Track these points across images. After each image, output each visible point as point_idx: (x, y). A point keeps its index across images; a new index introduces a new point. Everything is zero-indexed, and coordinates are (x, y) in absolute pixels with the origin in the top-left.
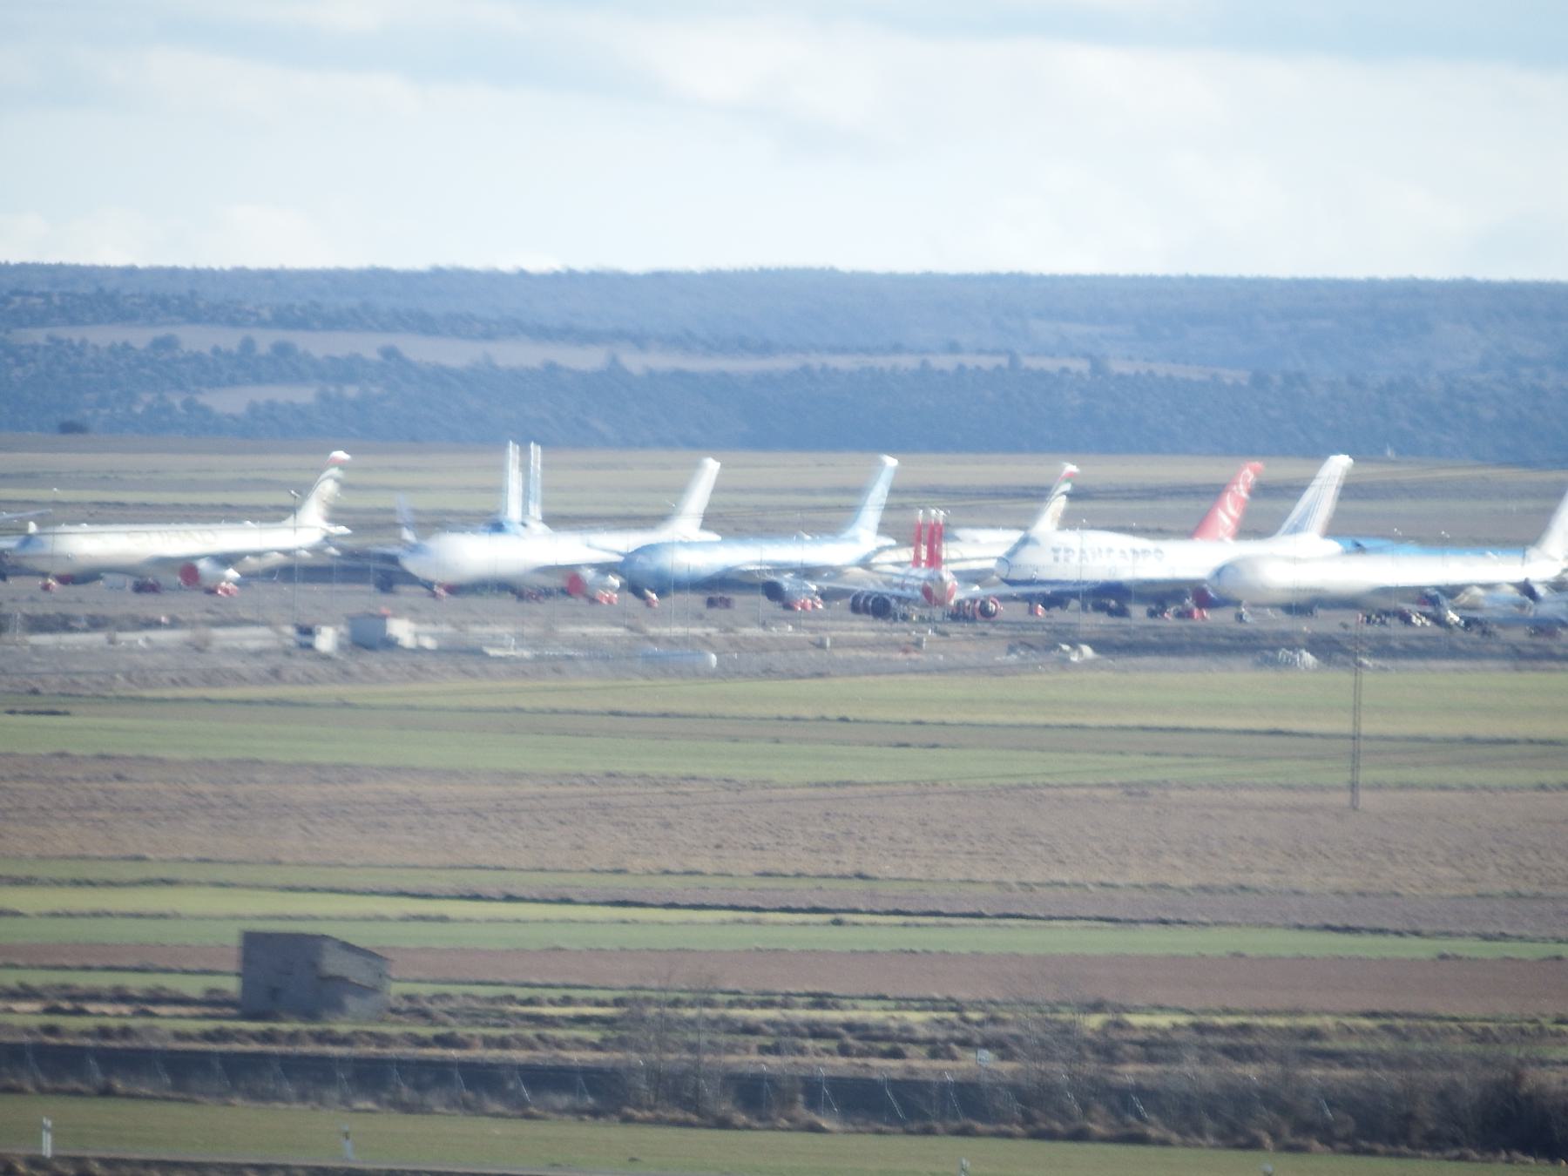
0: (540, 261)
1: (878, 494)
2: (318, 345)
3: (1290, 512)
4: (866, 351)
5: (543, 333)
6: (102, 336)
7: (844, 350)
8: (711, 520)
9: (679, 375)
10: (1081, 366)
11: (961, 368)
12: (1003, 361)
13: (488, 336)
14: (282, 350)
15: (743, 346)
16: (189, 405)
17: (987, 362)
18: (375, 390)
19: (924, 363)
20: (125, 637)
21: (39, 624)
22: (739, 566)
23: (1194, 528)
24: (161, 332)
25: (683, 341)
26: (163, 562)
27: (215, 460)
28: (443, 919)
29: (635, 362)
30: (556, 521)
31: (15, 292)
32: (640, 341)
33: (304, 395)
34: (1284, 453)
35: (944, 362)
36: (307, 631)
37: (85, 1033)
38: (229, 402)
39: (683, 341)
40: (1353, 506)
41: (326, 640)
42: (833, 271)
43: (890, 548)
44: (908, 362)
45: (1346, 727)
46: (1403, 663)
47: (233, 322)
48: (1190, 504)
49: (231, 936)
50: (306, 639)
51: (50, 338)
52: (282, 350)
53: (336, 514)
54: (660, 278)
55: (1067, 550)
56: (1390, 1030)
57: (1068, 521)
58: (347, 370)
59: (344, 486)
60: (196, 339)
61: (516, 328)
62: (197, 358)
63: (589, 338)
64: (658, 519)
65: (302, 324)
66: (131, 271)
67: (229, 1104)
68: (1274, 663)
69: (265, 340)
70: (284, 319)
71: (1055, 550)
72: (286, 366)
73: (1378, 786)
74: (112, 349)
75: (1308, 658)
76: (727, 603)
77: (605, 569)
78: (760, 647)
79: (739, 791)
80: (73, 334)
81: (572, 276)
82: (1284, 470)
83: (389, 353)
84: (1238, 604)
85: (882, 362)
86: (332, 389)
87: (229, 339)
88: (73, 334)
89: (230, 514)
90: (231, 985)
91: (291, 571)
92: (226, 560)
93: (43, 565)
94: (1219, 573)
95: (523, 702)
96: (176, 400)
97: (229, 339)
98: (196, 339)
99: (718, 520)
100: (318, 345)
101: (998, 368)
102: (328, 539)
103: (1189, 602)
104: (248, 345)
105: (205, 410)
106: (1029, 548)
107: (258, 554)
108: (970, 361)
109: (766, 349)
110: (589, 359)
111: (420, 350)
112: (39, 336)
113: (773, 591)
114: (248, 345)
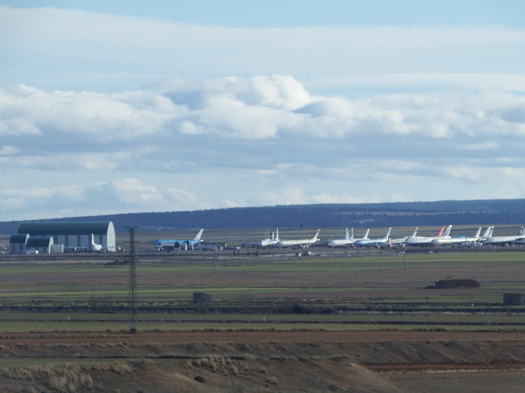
2: (374, 213)
4: (449, 211)
6: (345, 213)
7: (446, 211)
8: (368, 237)
9: (423, 216)
10: (478, 212)
11: (462, 213)
12: (467, 212)
13: (398, 211)
15: (432, 211)
16: (356, 222)
17: (465, 212)
18: (382, 219)
19: (414, 214)
20: (275, 255)
21: (263, 254)
22: (98, 245)
23: (473, 236)
27: (339, 230)
28: (253, 290)
29: (417, 214)
30: (330, 237)
32: (419, 211)
34: (425, 225)
35: (460, 213)
36: (297, 254)
37: (162, 306)
39: (425, 211)
40: (452, 232)
41: (300, 255)
42: (454, 200)
43: (369, 240)
44: (455, 213)
45: (403, 261)
46: (449, 252)
48: (437, 232)
49: (192, 294)
50: (297, 255)
51: (384, 214)
52: (370, 214)
53: (318, 238)
55: (414, 239)
56: (33, 301)
57: (417, 235)
58: (379, 217)
61: (401, 210)
63: (412, 211)
64: (362, 237)
66: (361, 204)
67: (215, 314)
68: (427, 253)
69: (367, 213)
70: (370, 210)
71: (413, 239)
72: (370, 216)
75: (432, 252)
76: (369, 248)
78: (361, 253)
79: (214, 272)
80: (341, 213)
82: (485, 226)
83: (384, 214)
84: (435, 245)
85: (451, 213)
86: (376, 220)
87: (363, 213)
88: (341, 213)
89: (305, 238)
90: (192, 299)
91: (313, 246)
92: (304, 244)
94: (432, 241)
96: (355, 222)
97: (363, 213)
98: (358, 213)
100: (374, 213)
102: (317, 241)
103: (431, 245)
104: (365, 214)
106: (409, 239)
108: (463, 212)
109: (435, 212)
110: (411, 214)
111: (388, 214)
112: (337, 214)
113: (375, 246)
114: (365, 214)
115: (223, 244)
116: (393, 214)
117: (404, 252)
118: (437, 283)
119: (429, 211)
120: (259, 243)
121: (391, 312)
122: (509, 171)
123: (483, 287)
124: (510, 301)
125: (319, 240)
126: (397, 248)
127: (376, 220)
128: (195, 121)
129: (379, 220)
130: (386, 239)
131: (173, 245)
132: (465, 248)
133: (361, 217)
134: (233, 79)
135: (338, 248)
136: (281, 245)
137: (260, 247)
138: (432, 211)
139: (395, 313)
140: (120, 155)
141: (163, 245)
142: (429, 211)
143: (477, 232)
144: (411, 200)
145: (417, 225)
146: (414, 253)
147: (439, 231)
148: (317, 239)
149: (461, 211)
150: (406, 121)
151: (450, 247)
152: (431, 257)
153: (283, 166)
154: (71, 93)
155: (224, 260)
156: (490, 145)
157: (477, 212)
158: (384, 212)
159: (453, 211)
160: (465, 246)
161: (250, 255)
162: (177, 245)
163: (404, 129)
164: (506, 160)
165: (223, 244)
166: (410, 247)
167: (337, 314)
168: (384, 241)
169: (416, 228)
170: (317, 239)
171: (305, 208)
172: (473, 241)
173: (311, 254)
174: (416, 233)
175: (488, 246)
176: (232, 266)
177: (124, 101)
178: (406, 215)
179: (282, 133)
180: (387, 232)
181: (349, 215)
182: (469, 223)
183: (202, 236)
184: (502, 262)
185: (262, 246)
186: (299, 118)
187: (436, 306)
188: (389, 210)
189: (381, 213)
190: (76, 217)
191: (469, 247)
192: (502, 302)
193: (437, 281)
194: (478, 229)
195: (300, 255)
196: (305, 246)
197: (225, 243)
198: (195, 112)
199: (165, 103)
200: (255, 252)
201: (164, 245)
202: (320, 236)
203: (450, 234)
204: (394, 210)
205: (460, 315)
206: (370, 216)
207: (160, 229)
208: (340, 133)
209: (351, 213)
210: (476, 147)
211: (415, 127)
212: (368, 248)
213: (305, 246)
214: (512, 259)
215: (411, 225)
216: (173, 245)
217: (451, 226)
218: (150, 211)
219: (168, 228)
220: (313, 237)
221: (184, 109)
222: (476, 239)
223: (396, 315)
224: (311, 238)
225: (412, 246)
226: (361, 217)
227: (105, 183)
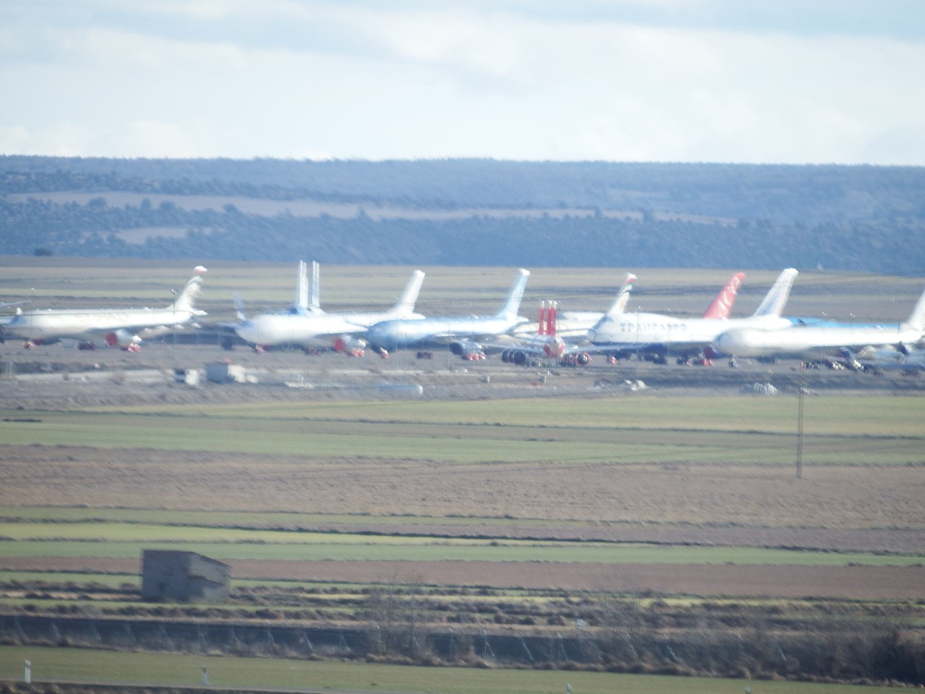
0: (319, 154)
1: (518, 292)
2: (187, 204)
3: (761, 302)
4: (511, 207)
5: (320, 197)
6: (60, 198)
7: (498, 207)
8: (419, 307)
9: (401, 221)
10: (637, 216)
11: (567, 217)
12: (592, 213)
13: (288, 198)
14: (167, 206)
15: (438, 204)
16: (112, 239)
17: (582, 214)
18: (221, 230)
19: (545, 214)
20: (74, 376)
21: (23, 368)
22: (436, 334)
23: (704, 312)
24: (95, 196)
25: (403, 201)
26: (96, 332)
27: (127, 271)
28: (261, 542)
29: (375, 214)
30: (328, 307)
31: (9, 173)
32: (377, 201)
33: (179, 233)
34: (758, 267)
35: (557, 214)
36: (181, 372)
37: (50, 610)
38: (135, 237)
39: (403, 201)
40: (798, 298)
41: (192, 378)
42: (491, 160)
43: (525, 323)
44: (536, 214)
45: (794, 429)
46: (828, 391)
47: (137, 190)
48: (702, 298)
49: (136, 553)
50: (180, 377)
51: (30, 200)
52: (167, 206)
53: (198, 303)
54: (389, 164)
55: (630, 325)
57: (630, 308)
58: (205, 218)
59: (203, 287)
60: (115, 200)
61: (305, 194)
62: (116, 211)
63: (347, 199)
64: (388, 306)
65: (178, 191)
66: (77, 160)
67: (135, 652)
68: (752, 391)
69: (156, 201)
70: (167, 188)
71: (623, 325)
72: (168, 216)
73: (813, 464)
74: (66, 206)
75: (772, 388)
76: (429, 356)
78: (449, 382)
79: (436, 467)
80: (43, 197)
81: (337, 163)
82: (757, 277)
83: (230, 208)
84: (730, 356)
85: (521, 214)
86: (196, 230)
87: (135, 200)
88: (43, 197)
89: (136, 303)
90: (136, 581)
91: (172, 337)
92: (133, 330)
93: (26, 334)
94: (719, 338)
95: (309, 415)
96: (104, 236)
97: (135, 200)
98: (115, 200)
99: (423, 307)
100: (187, 204)
101: (589, 217)
102: (193, 318)
104: (146, 204)
105: (121, 242)
106: (607, 324)
107: (152, 327)
108: (572, 213)
109: (452, 206)
110: (347, 212)
111: (248, 206)
112: (23, 198)
113: (456, 349)
114: (146, 204)
117: (641, 384)
147: (717, 290)
212: (419, 356)
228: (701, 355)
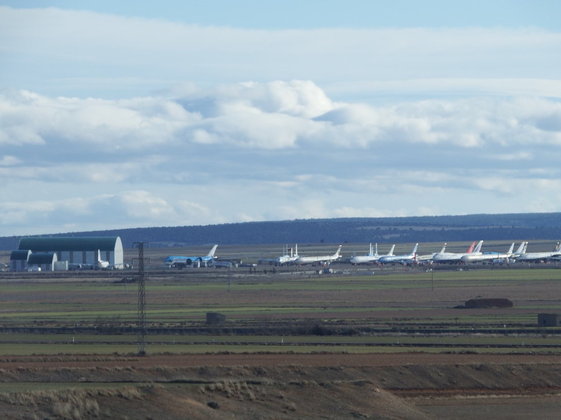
2: (400, 228)
4: (479, 226)
6: (369, 228)
7: (476, 226)
8: (394, 254)
9: (452, 230)
10: (511, 227)
11: (493, 228)
12: (499, 227)
13: (425, 226)
15: (462, 226)
16: (381, 237)
17: (497, 227)
18: (409, 234)
19: (443, 229)
20: (294, 273)
21: (281, 271)
22: (104, 262)
23: (505, 252)
27: (363, 246)
28: (270, 310)
29: (446, 229)
30: (353, 253)
32: (447, 226)
34: (454, 241)
35: (491, 227)
36: (318, 271)
37: (173, 327)
39: (454, 226)
40: (483, 248)
41: (320, 272)
42: (485, 214)
43: (394, 256)
44: (486, 227)
45: (431, 279)
46: (480, 270)
48: (467, 248)
49: (205, 314)
50: (318, 272)
51: (410, 229)
52: (395, 229)
53: (340, 254)
55: (443, 255)
57: (445, 251)
58: (405, 231)
61: (429, 225)
63: (440, 226)
64: (387, 253)
66: (385, 218)
67: (230, 335)
68: (456, 270)
69: (393, 228)
70: (396, 225)
71: (441, 256)
72: (395, 231)
75: (461, 270)
76: (395, 265)
77: (431, 260)
78: (386, 271)
79: (228, 291)
80: (365, 228)
82: (518, 242)
83: (410, 229)
84: (465, 262)
85: (482, 227)
86: (402, 235)
87: (388, 228)
88: (365, 228)
89: (326, 255)
90: (205, 320)
91: (334, 263)
92: (325, 261)
94: (462, 258)
96: (380, 237)
97: (388, 228)
98: (383, 228)
100: (400, 228)
102: (339, 258)
104: (390, 229)
106: (437, 256)
108: (495, 227)
109: (465, 226)
110: (439, 229)
111: (415, 228)
112: (360, 228)
113: (401, 263)
114: (390, 229)
115: (238, 261)
116: (420, 229)
118: (467, 303)
119: (458, 226)
120: (277, 260)
121: (418, 334)
122: (544, 182)
123: (516, 307)
124: (545, 322)
125: (341, 256)
126: (424, 266)
127: (402, 235)
128: (209, 129)
129: (405, 235)
130: (413, 255)
131: (185, 262)
132: (497, 265)
133: (386, 232)
134: (249, 84)
135: (361, 265)
136: (300, 262)
137: (278, 264)
138: (462, 226)
139: (423, 334)
140: (128, 165)
141: (174, 262)
142: (458, 226)
143: (509, 248)
144: (439, 214)
145: (445, 241)
146: (442, 271)
148: (339, 255)
149: (493, 225)
150: (434, 129)
151: (481, 264)
152: (461, 274)
153: (303, 178)
154: (75, 99)
155: (239, 277)
156: (524, 155)
157: (510, 227)
158: (411, 227)
159: (484, 225)
160: (497, 262)
161: (267, 273)
162: (189, 262)
163: (432, 138)
164: (540, 171)
165: (238, 261)
166: (438, 264)
167: (360, 335)
168: (410, 257)
169: (444, 244)
170: (339, 255)
171: (326, 222)
172: (505, 258)
173: (332, 272)
174: (444, 249)
175: (522, 263)
176: (248, 284)
177: (132, 108)
178: (434, 230)
179: (301, 142)
180: (414, 248)
181: (373, 229)
182: (501, 238)
183: (216, 252)
184: (537, 280)
185: (280, 263)
186: (320, 126)
187: (466, 327)
188: (416, 225)
189: (407, 228)
190: (81, 232)
191: (501, 264)
192: (536, 322)
193: (467, 300)
194: (510, 245)
195: (320, 272)
196: (325, 263)
197: (240, 260)
198: (209, 120)
199: (177, 110)
200: (272, 270)
201: (176, 262)
202: (342, 252)
203: (480, 250)
204: (421, 224)
205: (492, 337)
206: (395, 231)
207: (171, 244)
208: (363, 143)
209: (375, 228)
210: (509, 157)
211: (444, 136)
213: (325, 263)
214: (547, 277)
215: (439, 241)
216: (185, 262)
217: (482, 241)
218: (160, 225)
219: (180, 244)
220: (335, 253)
221: (197, 117)
222: (509, 256)
223: (423, 336)
224: (333, 254)
225: (441, 263)
226: (386, 232)
227: (112, 196)
228: (460, 262)
